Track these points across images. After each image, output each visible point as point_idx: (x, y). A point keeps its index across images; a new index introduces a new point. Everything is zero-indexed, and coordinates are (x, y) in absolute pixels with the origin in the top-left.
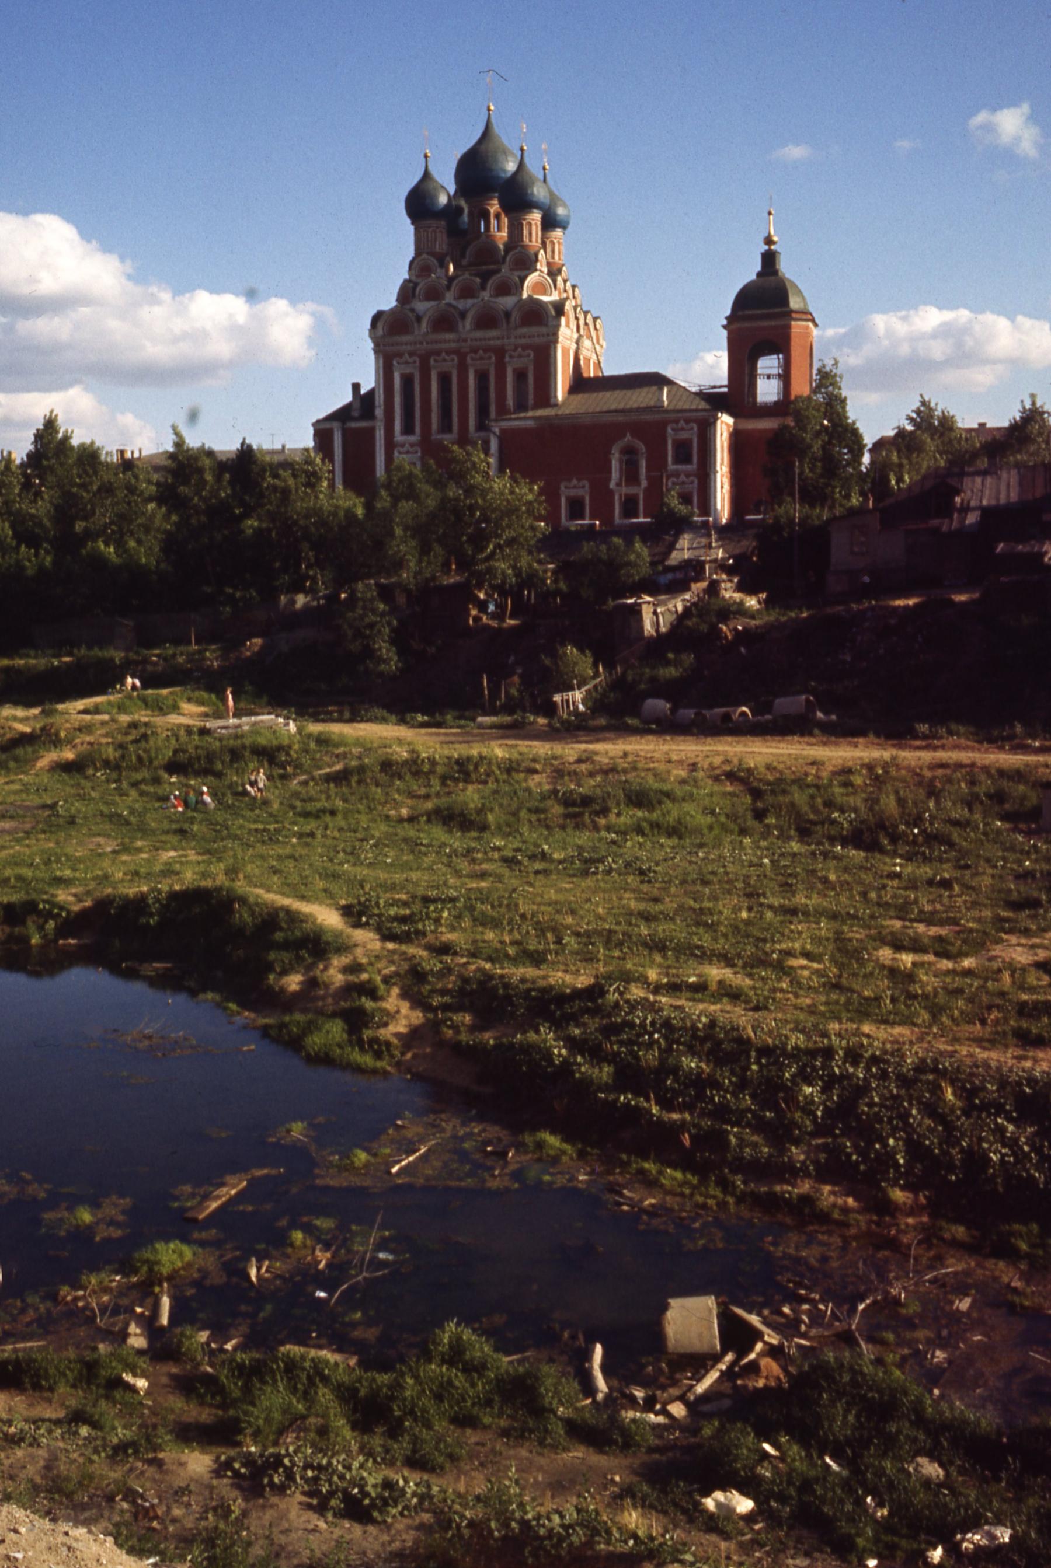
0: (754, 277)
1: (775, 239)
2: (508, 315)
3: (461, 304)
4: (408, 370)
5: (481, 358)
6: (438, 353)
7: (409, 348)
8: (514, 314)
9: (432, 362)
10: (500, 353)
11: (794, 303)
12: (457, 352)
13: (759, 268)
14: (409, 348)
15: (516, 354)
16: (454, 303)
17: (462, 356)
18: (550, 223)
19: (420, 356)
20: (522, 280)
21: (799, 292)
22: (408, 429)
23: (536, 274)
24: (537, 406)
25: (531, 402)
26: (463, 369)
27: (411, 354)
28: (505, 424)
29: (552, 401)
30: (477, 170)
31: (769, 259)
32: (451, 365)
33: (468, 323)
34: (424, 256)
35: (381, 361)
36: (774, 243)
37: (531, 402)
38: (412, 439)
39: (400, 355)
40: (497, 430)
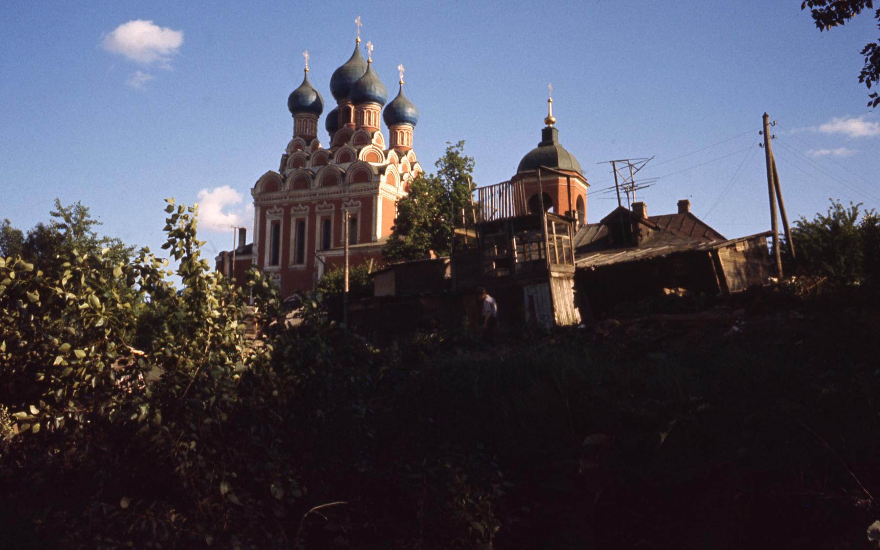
0: (536, 146)
1: (553, 119)
2: (344, 175)
3: (316, 169)
4: (276, 218)
5: (325, 208)
6: (296, 205)
7: (277, 201)
8: (349, 174)
9: (292, 211)
10: (338, 203)
11: (562, 164)
12: (308, 203)
13: (540, 140)
14: (277, 201)
15: (349, 204)
16: (311, 168)
17: (312, 206)
18: (394, 117)
19: (284, 207)
20: (359, 151)
21: (568, 156)
22: (274, 262)
23: (371, 146)
24: (362, 242)
25: (358, 239)
26: (312, 216)
27: (279, 206)
28: (329, 253)
29: (373, 239)
30: (350, 88)
31: (548, 134)
32: (304, 213)
33: (317, 182)
34: (298, 138)
35: (259, 211)
36: (553, 123)
37: (358, 239)
38: (276, 268)
39: (271, 207)
40: (323, 258)
